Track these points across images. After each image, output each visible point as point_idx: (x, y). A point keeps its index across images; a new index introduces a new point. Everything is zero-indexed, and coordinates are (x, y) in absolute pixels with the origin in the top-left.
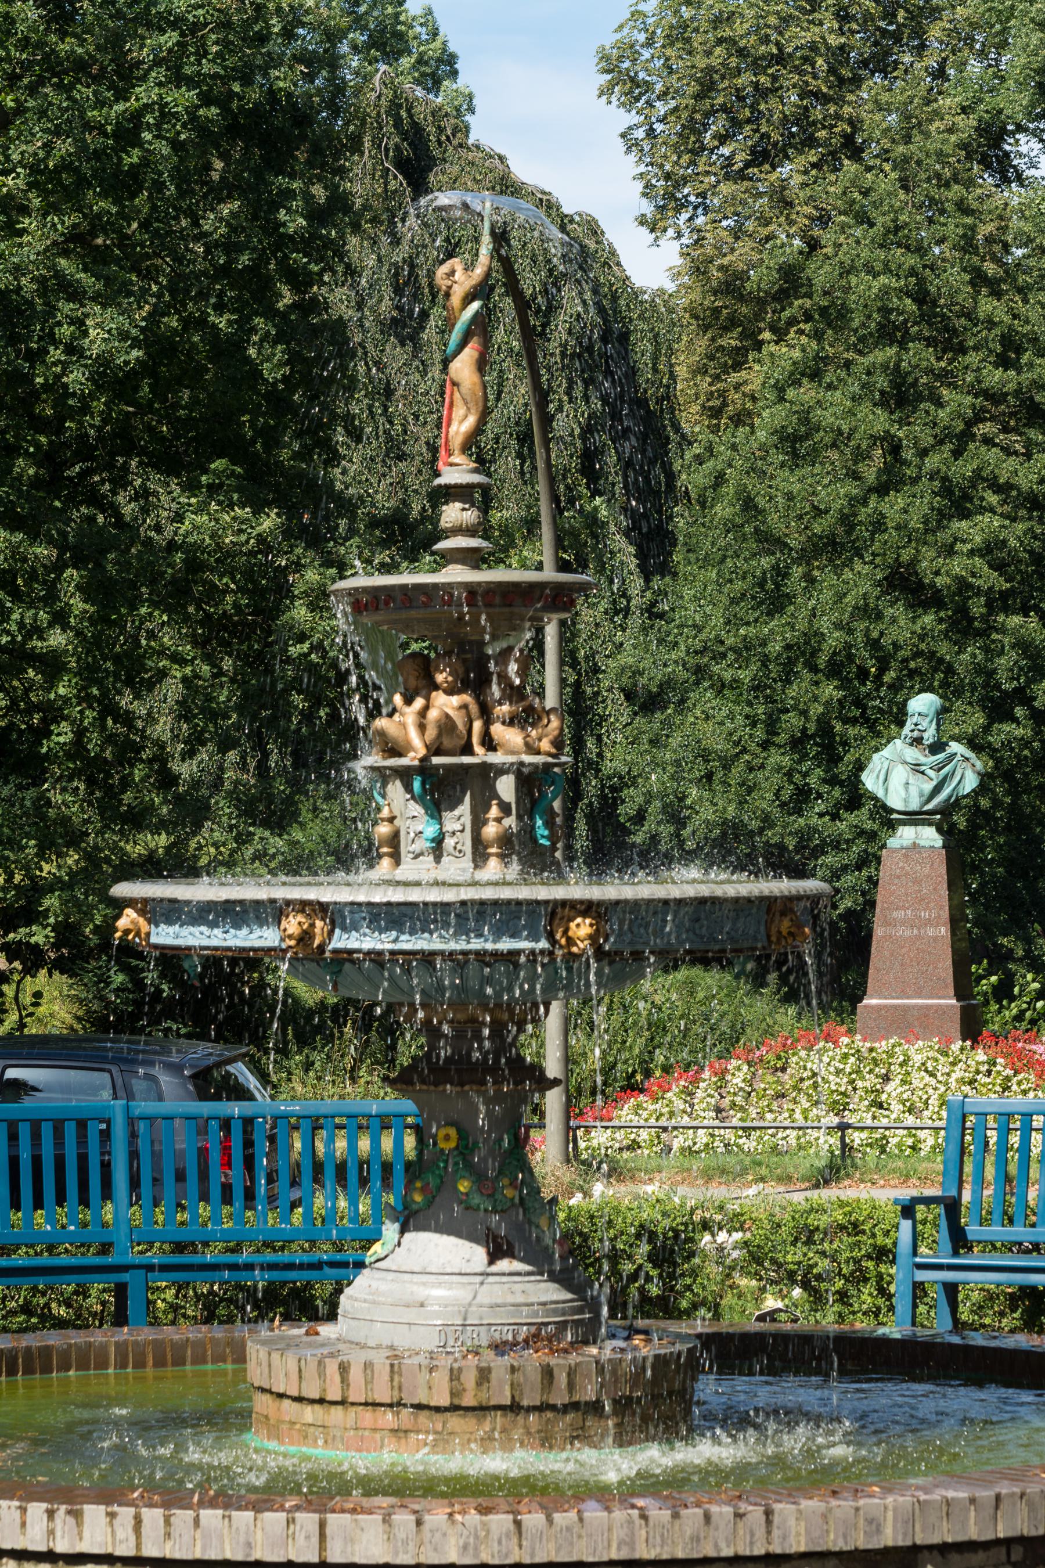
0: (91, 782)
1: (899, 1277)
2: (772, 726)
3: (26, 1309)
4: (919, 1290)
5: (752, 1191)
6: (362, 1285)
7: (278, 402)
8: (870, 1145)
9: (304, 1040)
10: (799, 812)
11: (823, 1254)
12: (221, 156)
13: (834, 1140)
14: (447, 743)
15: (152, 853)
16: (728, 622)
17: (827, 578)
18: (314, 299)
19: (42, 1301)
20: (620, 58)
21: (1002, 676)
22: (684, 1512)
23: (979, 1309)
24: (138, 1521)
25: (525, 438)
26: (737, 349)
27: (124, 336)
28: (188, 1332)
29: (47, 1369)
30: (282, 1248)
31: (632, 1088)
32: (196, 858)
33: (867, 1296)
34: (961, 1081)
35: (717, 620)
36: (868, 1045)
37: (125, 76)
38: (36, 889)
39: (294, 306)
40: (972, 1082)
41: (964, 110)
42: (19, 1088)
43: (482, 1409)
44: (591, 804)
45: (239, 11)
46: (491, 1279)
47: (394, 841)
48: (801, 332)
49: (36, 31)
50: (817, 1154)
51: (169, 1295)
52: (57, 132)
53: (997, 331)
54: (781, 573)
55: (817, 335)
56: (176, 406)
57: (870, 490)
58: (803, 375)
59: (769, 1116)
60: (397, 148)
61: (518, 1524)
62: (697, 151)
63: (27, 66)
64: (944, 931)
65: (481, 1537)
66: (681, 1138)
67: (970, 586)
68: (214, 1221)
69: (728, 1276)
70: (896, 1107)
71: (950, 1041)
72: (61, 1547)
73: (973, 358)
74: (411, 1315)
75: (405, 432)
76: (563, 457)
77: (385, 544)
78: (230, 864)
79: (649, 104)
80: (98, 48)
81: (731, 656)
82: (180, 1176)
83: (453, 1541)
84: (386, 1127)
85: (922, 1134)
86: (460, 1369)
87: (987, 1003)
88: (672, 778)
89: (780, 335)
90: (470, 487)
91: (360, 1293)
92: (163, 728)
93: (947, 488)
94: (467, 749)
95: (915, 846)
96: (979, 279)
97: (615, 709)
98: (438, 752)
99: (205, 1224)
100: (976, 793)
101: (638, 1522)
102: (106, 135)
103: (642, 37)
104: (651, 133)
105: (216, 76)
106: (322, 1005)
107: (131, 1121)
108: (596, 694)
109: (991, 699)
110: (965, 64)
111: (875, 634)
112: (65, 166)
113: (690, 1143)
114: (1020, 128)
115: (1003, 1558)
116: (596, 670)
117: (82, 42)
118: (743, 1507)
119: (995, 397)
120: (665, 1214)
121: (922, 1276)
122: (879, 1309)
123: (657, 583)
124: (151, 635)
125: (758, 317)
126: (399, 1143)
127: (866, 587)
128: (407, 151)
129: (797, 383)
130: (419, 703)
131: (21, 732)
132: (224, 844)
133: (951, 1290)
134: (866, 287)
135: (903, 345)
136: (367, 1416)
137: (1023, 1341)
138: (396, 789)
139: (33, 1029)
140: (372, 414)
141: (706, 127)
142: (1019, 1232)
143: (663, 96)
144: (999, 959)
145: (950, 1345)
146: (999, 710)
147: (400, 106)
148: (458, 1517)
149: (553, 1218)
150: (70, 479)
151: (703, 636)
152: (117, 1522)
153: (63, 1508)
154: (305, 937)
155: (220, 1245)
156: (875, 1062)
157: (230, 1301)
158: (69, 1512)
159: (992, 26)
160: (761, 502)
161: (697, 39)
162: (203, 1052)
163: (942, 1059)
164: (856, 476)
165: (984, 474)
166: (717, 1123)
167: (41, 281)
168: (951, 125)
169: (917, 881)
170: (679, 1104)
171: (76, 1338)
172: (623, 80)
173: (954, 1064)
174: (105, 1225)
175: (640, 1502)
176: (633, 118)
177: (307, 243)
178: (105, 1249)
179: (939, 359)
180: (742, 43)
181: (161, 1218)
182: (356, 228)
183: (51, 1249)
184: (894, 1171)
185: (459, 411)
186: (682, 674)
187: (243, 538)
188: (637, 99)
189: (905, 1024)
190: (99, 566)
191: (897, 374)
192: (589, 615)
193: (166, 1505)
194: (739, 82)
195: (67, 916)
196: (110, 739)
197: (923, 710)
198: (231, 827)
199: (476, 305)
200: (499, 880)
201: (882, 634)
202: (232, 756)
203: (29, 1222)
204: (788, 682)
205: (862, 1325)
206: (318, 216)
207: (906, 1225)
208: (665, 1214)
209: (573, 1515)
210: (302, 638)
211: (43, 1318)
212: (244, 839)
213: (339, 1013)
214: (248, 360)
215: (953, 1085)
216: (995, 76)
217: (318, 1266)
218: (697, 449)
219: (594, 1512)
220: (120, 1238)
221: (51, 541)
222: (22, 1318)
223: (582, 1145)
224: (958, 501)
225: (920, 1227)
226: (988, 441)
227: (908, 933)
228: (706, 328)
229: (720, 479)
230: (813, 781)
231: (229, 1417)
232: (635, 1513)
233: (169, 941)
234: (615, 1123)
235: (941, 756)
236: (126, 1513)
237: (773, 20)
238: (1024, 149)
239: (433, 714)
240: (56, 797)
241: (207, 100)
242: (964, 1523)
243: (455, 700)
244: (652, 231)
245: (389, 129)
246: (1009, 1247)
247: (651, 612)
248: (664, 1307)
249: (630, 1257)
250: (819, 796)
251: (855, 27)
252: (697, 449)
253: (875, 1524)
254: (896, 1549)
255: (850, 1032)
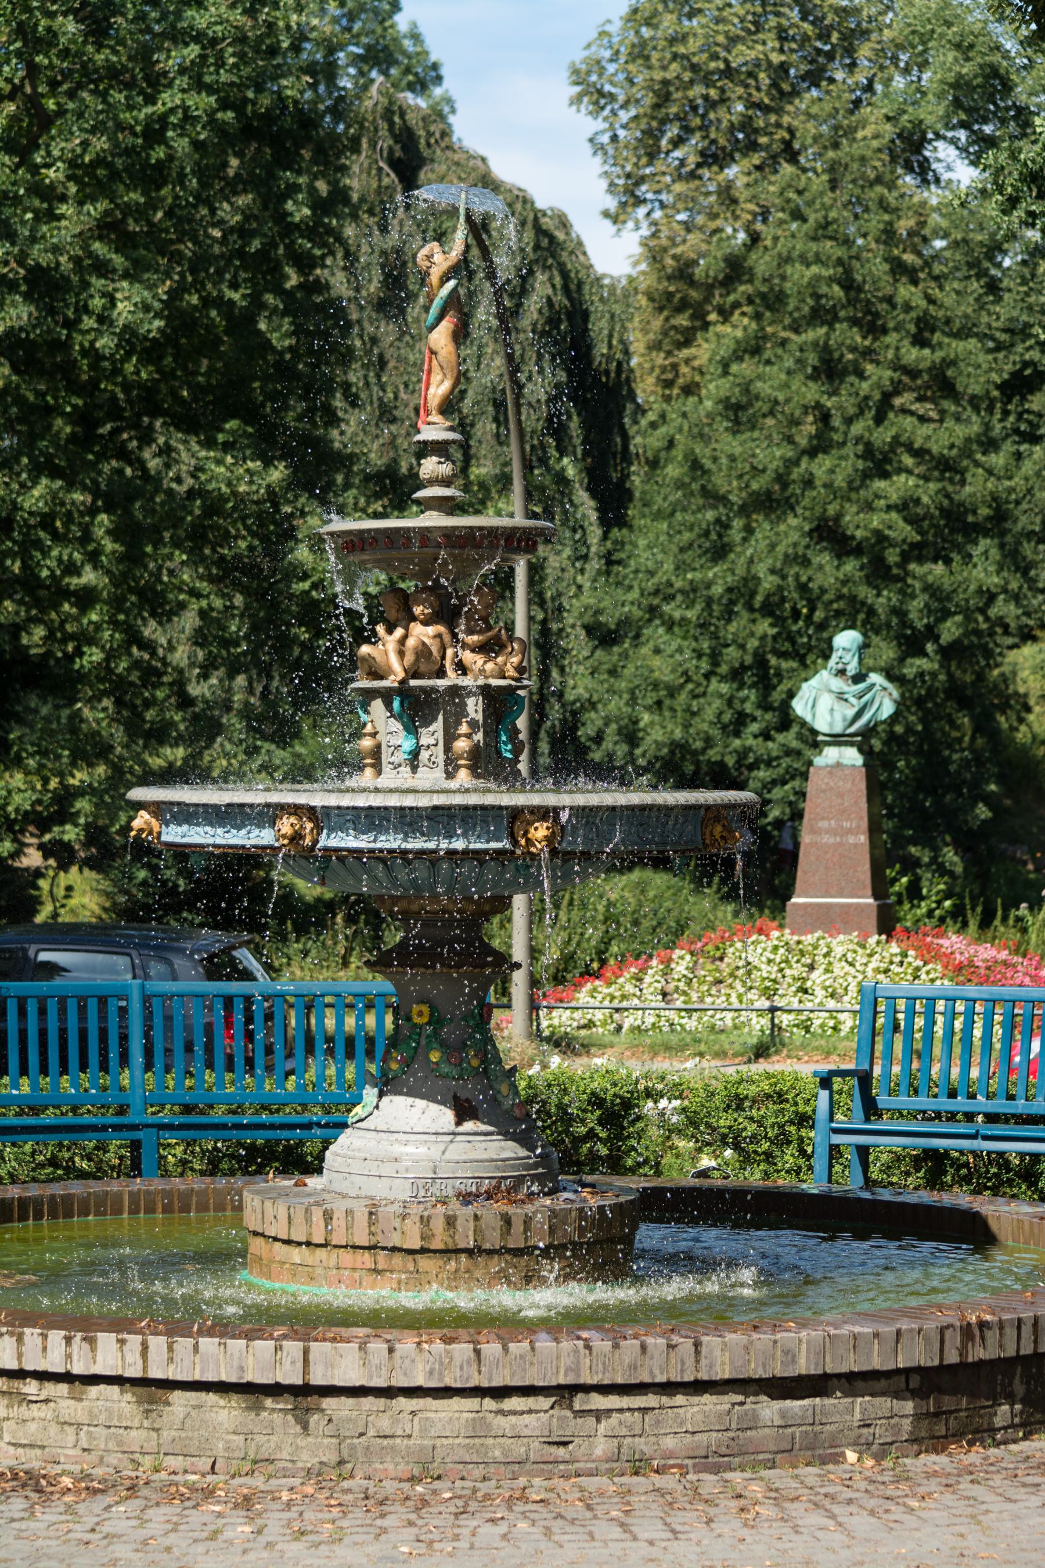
0: (119, 703)
1: (817, 1137)
2: (715, 658)
3: (54, 1162)
4: (835, 1152)
5: (689, 1064)
6: (344, 1144)
7: (284, 370)
8: (797, 1026)
9: (301, 930)
10: (737, 734)
11: (751, 1119)
12: (236, 155)
13: (765, 1021)
14: (423, 668)
15: (171, 765)
16: (677, 568)
17: (763, 528)
18: (317, 280)
19: (67, 1155)
20: (589, 73)
21: (913, 615)
22: (623, 1343)
23: (887, 1169)
24: (145, 1347)
25: (499, 405)
26: (687, 329)
27: (147, 308)
28: (196, 1183)
29: (69, 1215)
30: (278, 1111)
31: (588, 974)
32: (210, 769)
33: (789, 1157)
34: (877, 971)
35: (668, 566)
36: (796, 938)
37: (156, 82)
38: (66, 797)
39: (300, 286)
40: (886, 971)
41: (888, 119)
42: (52, 970)
43: (449, 1252)
44: (553, 726)
45: (253, 28)
46: (459, 1138)
47: (376, 752)
48: (744, 314)
49: (75, 42)
50: (750, 1033)
51: (179, 1150)
52: (93, 131)
53: (913, 314)
54: (723, 525)
55: (758, 317)
56: (196, 373)
57: (804, 452)
58: (745, 351)
59: (709, 1000)
60: (391, 149)
61: (478, 1352)
62: (652, 156)
63: (67, 75)
64: (863, 839)
65: (445, 1364)
66: (631, 1019)
67: (886, 538)
68: (223, 1088)
69: (668, 1138)
70: (820, 993)
71: (867, 936)
72: (77, 1369)
73: (892, 338)
74: (388, 1169)
75: (396, 398)
76: (533, 420)
77: (377, 496)
78: (241, 776)
79: (614, 113)
80: (130, 58)
81: (679, 598)
82: (189, 1048)
83: (420, 1367)
84: (369, 1006)
85: (842, 1017)
86: (429, 1217)
87: (900, 902)
88: (627, 704)
89: (725, 314)
90: (446, 443)
91: (344, 1151)
92: (180, 656)
93: (869, 452)
94: (441, 673)
95: (838, 765)
96: (899, 269)
97: (577, 643)
98: (416, 675)
99: (210, 1089)
100: (894, 718)
101: (583, 1351)
102: (135, 135)
103: (607, 54)
104: (614, 138)
105: (232, 84)
106: (319, 900)
107: (147, 1000)
108: (561, 630)
109: (905, 636)
110: (890, 79)
111: (804, 579)
112: (99, 161)
113: (639, 1022)
114: (938, 136)
115: (903, 1385)
116: (560, 609)
117: (115, 52)
118: (676, 1339)
119: (913, 373)
120: (615, 1084)
121: (837, 1139)
122: (800, 1168)
123: (615, 533)
124: (171, 573)
125: (707, 300)
126: (380, 1022)
127: (795, 536)
128: (398, 153)
129: (741, 359)
130: (399, 632)
131: (57, 660)
132: (235, 756)
133: (863, 1151)
134: (800, 275)
135: (831, 325)
136: (347, 1257)
137: (927, 1197)
138: (377, 706)
139: (65, 917)
140: (367, 384)
141: (663, 133)
142: (923, 1102)
143: (625, 106)
144: (910, 865)
145: (860, 1200)
146: (912, 644)
147: (393, 113)
148: (425, 1346)
149: (514, 1086)
150: (102, 436)
151: (655, 580)
152: (126, 1348)
153: (79, 1335)
154: (296, 837)
155: (224, 1108)
156: (802, 953)
157: (232, 1156)
158: (84, 1339)
159: (914, 47)
160: (708, 464)
161: (655, 56)
162: (212, 939)
163: (860, 951)
164: (790, 440)
165: (902, 439)
166: (663, 1005)
167: (77, 260)
168: (874, 128)
169: (840, 795)
170: (629, 988)
171: (95, 1187)
172: (594, 96)
173: (871, 955)
174: (122, 1089)
175: (585, 1334)
176: (600, 124)
177: (314, 231)
178: (122, 1111)
179: (864, 338)
180: (695, 60)
181: (171, 1083)
182: (355, 217)
183: (75, 1109)
184: (817, 1048)
185: (436, 377)
186: (637, 613)
187: (254, 488)
188: (603, 108)
189: (830, 920)
190: (128, 512)
191: (825, 350)
192: (556, 559)
193: (169, 1333)
194: (691, 94)
195: (96, 816)
196: (136, 664)
197: (847, 645)
198: (241, 741)
199: (452, 283)
200: (465, 789)
201: (810, 579)
202: (241, 680)
203: (56, 1085)
204: (729, 621)
205: (784, 1181)
206: (322, 206)
207: (824, 1095)
208: (615, 1084)
209: (525, 1345)
210: (305, 576)
211: (67, 1169)
212: (252, 752)
213: (330, 907)
214: (259, 331)
215: (870, 973)
216: (918, 90)
217: (308, 1126)
218: (651, 416)
219: (544, 1343)
220: (136, 1101)
221: (85, 489)
222: (50, 1170)
223: (545, 1024)
224: (879, 463)
225: (836, 1097)
226: (905, 411)
227: (832, 840)
228: (661, 309)
229: (671, 444)
230: (748, 708)
231: (223, 1258)
232: (581, 1343)
233: (178, 840)
234: (573, 1004)
235: (862, 686)
236: (134, 1341)
237: (721, 39)
238: (941, 155)
239: (411, 642)
240: (87, 712)
241: (224, 104)
242: (869, 1354)
243: (431, 630)
244: (615, 222)
245: (384, 132)
246: (913, 1115)
247: (610, 561)
248: (615, 1164)
249: (583, 1121)
250: (754, 719)
251: (794, 46)
252: (651, 416)
253: (791, 1356)
254: (809, 1377)
255: (781, 927)
